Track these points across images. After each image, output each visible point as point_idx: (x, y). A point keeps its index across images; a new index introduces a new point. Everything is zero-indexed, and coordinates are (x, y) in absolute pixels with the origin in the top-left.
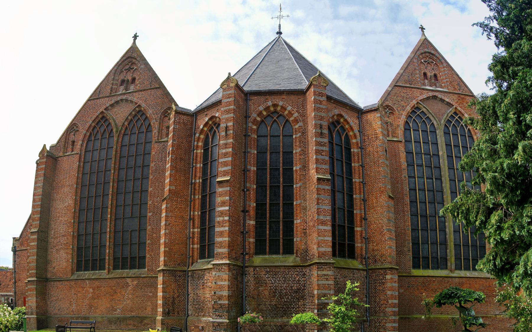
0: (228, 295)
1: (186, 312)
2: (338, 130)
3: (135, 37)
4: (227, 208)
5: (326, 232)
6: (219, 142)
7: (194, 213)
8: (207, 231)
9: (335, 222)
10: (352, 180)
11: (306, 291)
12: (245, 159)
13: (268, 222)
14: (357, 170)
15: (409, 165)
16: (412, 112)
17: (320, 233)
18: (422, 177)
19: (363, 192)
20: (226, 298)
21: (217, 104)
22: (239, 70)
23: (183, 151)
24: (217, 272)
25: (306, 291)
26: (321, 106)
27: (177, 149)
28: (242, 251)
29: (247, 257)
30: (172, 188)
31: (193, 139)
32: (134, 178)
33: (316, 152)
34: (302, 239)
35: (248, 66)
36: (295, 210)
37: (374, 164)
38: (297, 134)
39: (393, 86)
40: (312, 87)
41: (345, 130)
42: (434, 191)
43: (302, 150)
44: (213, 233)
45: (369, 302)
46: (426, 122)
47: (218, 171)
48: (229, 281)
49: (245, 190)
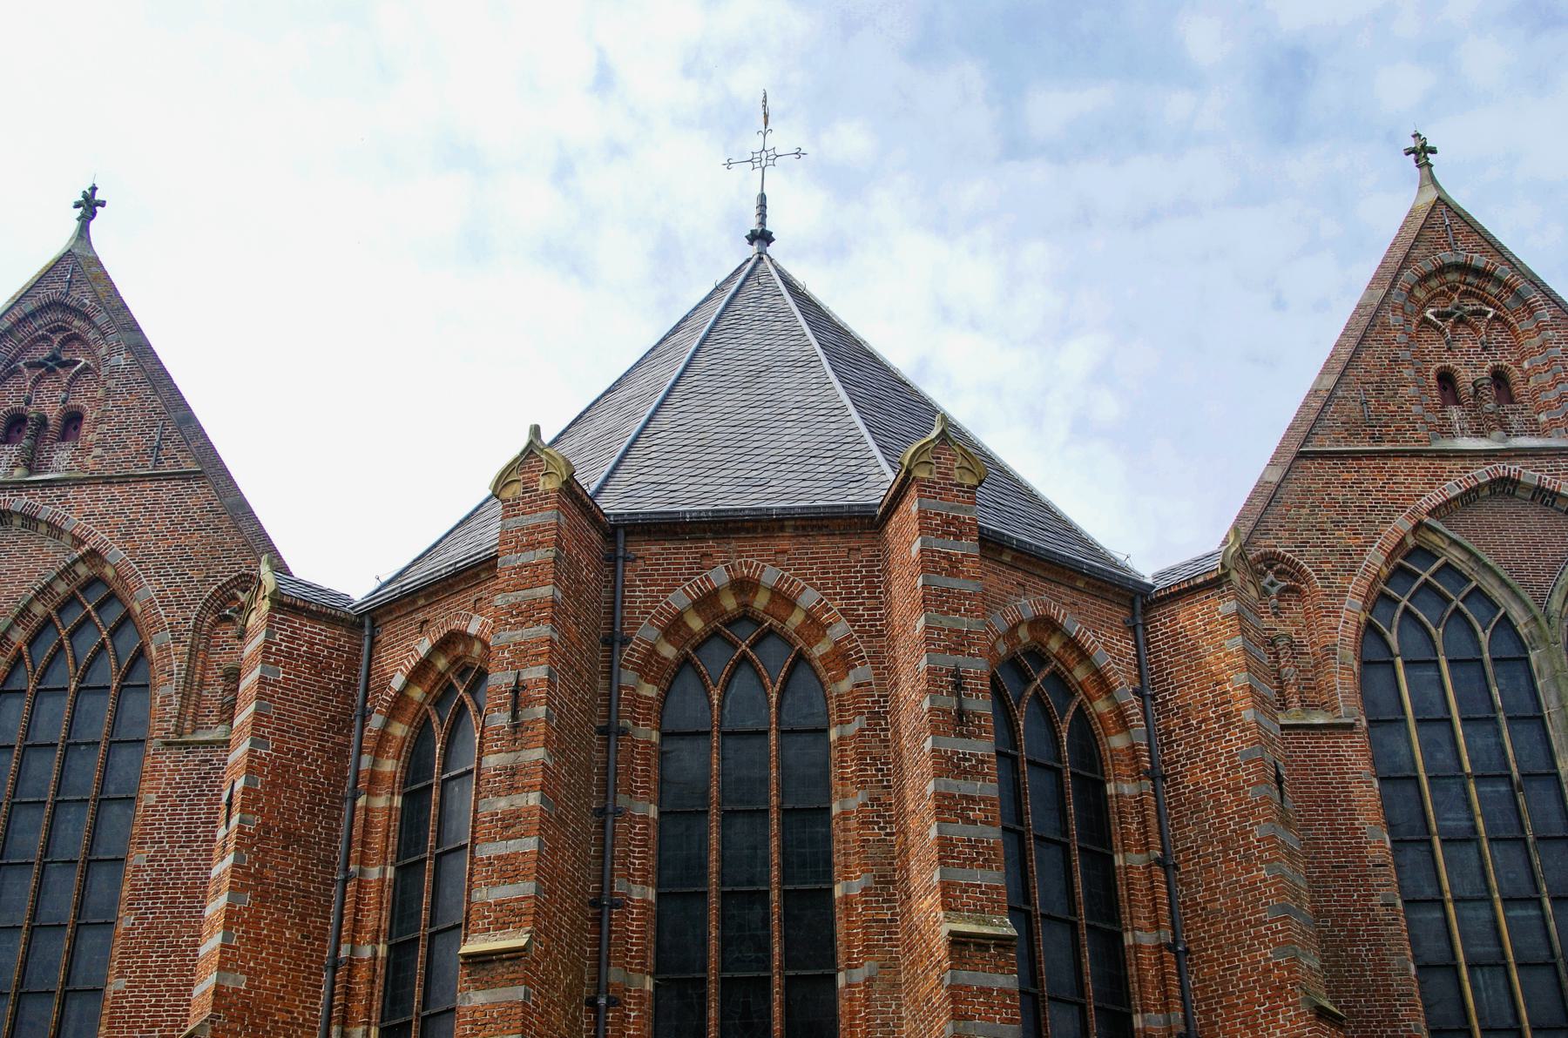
2: (1036, 692)
3: (89, 205)
6: (480, 759)
12: (604, 846)
14: (1141, 884)
15: (1402, 841)
16: (1392, 575)
18: (1482, 899)
21: (477, 575)
22: (580, 417)
23: (302, 795)
26: (955, 583)
27: (273, 784)
30: (230, 984)
31: (355, 739)
32: (33, 917)
33: (938, 807)
35: (620, 396)
37: (1225, 852)
38: (849, 722)
39: (1289, 458)
40: (913, 492)
42: (1555, 966)
43: (874, 800)
46: (1471, 617)
47: (469, 902)
49: (602, 1001)
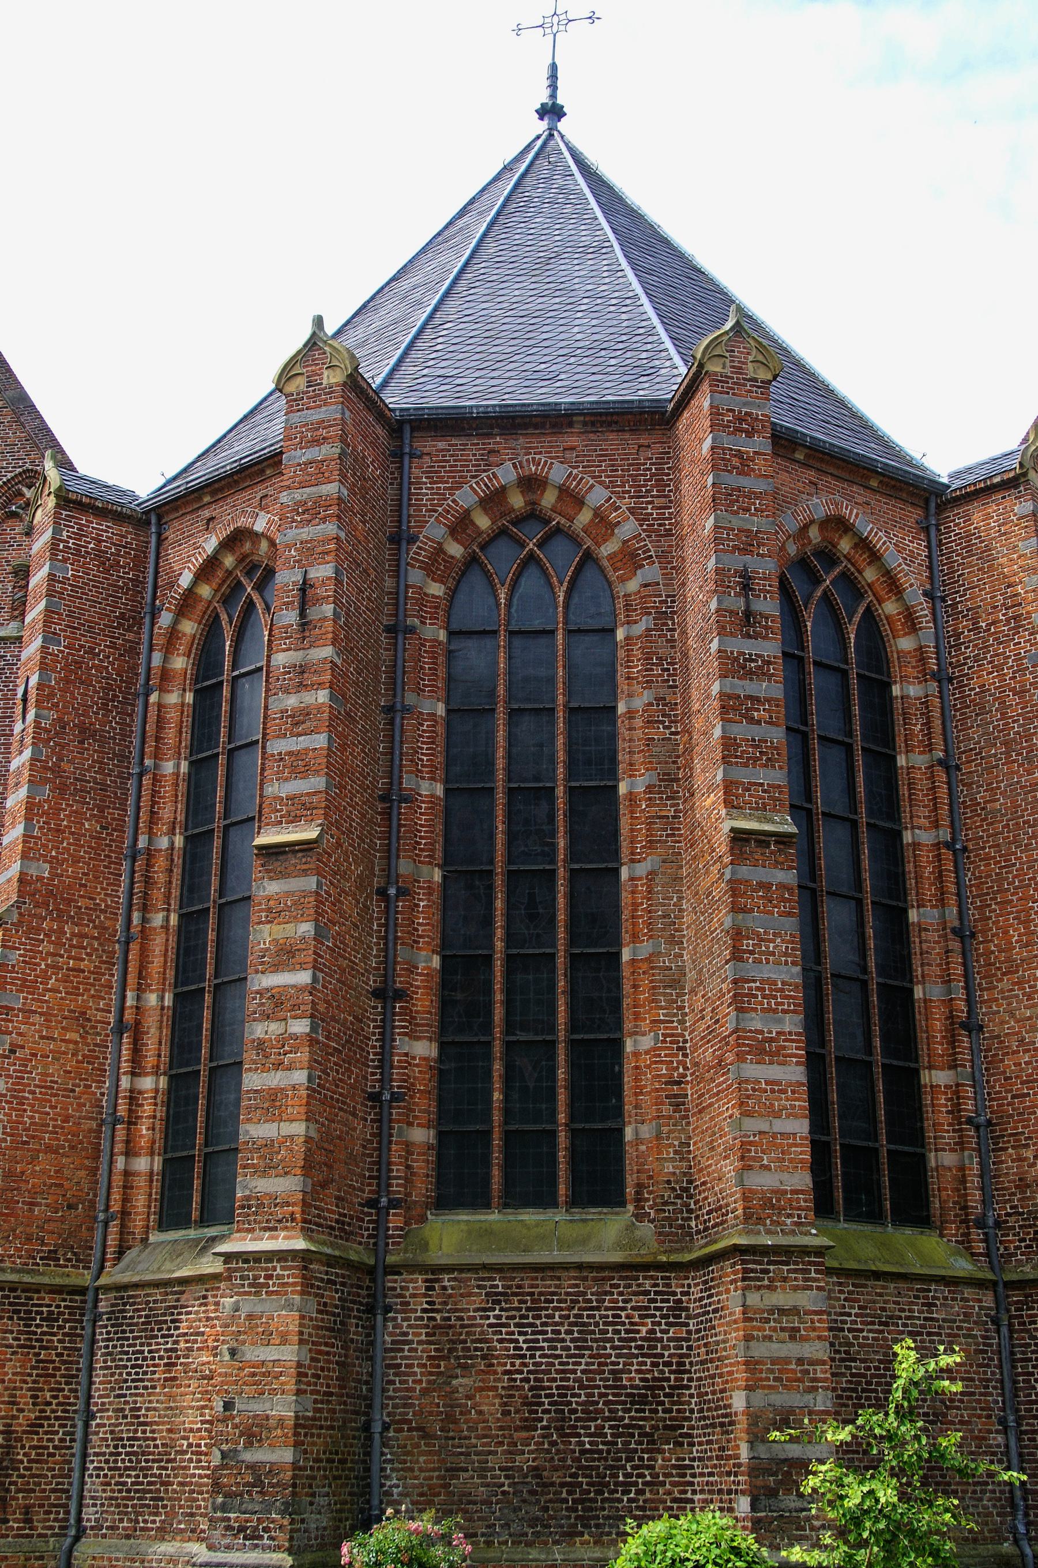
0: (297, 1417)
1: (67, 1513)
2: (825, 593)
4: (304, 977)
5: (781, 1091)
6: (269, 657)
7: (138, 998)
8: (202, 1089)
9: (823, 1043)
10: (899, 835)
11: (691, 1396)
12: (392, 742)
13: (497, 1048)
14: (923, 784)
17: (748, 1097)
19: (958, 895)
20: (286, 1436)
22: (364, 306)
24: (249, 1293)
25: (691, 1396)
26: (746, 482)
28: (370, 1192)
29: (395, 1220)
30: (33, 872)
31: (145, 637)
34: (665, 1129)
35: (405, 284)
36: (627, 987)
37: (1008, 754)
38: (636, 622)
40: (705, 387)
41: (859, 595)
44: (232, 1097)
45: (1021, 1455)
47: (261, 796)
48: (301, 1342)
49: (392, 891)
